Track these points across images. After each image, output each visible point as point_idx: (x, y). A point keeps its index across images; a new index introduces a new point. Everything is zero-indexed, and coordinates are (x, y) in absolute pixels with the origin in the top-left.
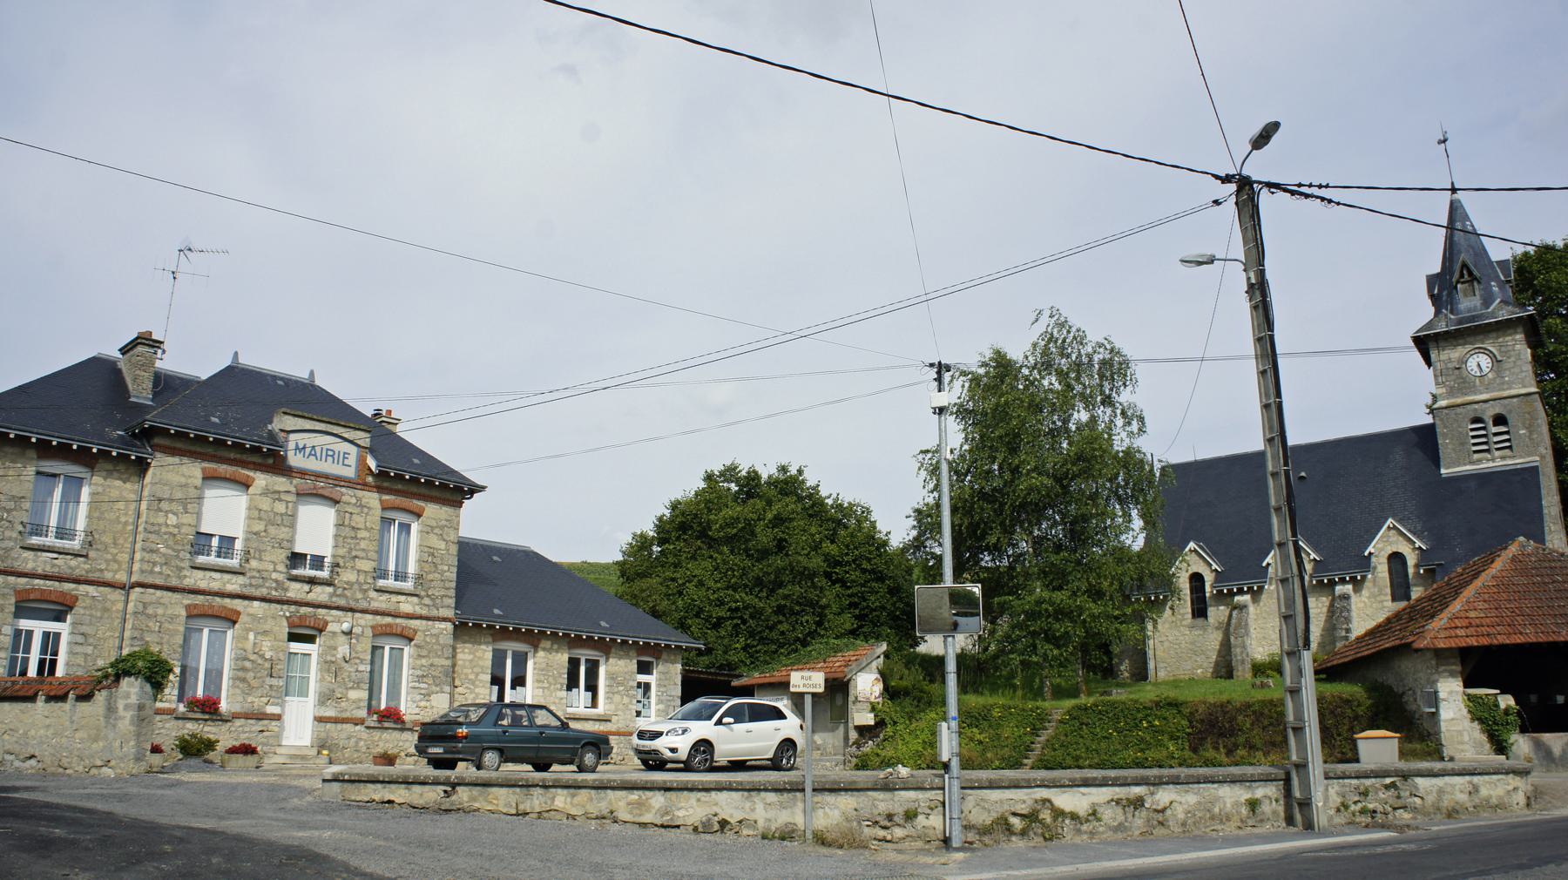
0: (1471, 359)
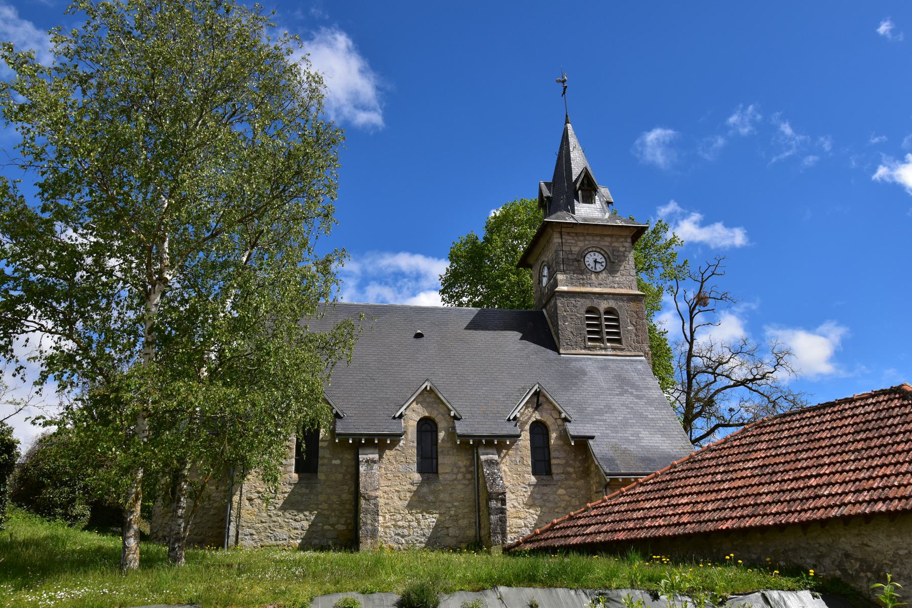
0: (588, 256)
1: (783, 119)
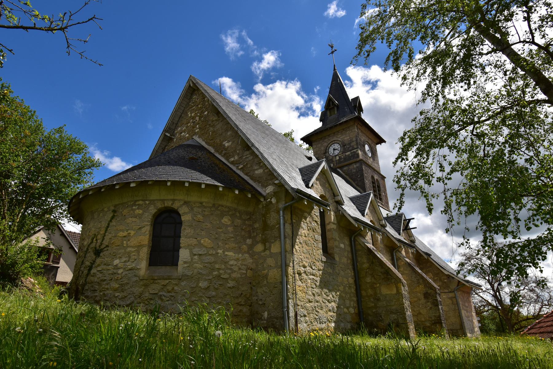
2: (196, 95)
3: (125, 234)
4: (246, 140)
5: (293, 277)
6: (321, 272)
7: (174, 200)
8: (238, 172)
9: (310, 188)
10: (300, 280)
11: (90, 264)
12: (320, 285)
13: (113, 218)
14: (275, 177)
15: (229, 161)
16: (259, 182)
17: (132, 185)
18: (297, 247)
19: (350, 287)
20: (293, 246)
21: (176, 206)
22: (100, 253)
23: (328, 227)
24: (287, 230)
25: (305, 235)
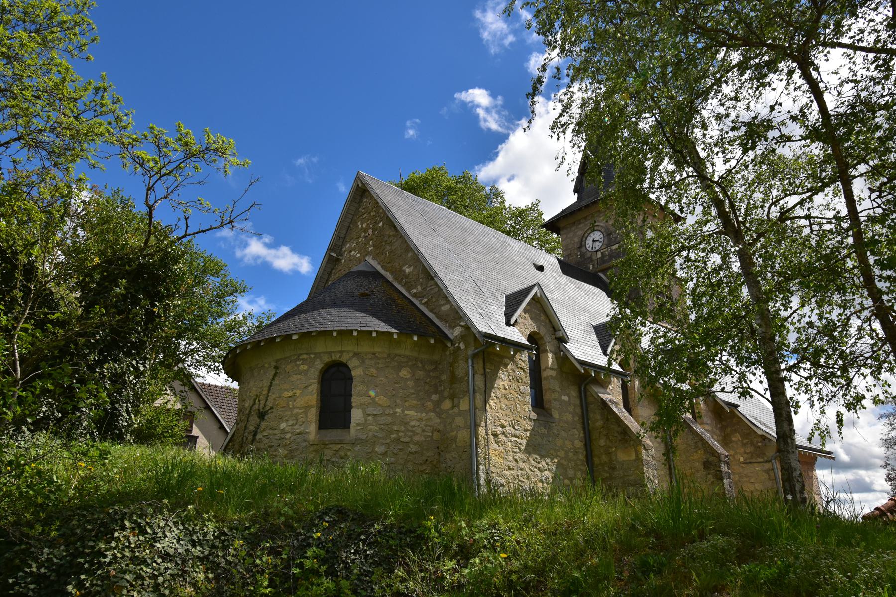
1: (843, 146)
2: (367, 197)
3: (290, 393)
4: (428, 268)
5: (485, 439)
6: (528, 434)
7: (342, 352)
8: (422, 308)
9: (513, 325)
10: (496, 443)
11: (254, 429)
12: (526, 449)
13: (275, 375)
14: (461, 318)
15: (410, 293)
16: (446, 322)
17: (295, 337)
18: (491, 402)
19: (576, 453)
20: (486, 402)
21: (344, 359)
22: (264, 416)
23: (544, 374)
24: (477, 383)
25: (504, 386)
